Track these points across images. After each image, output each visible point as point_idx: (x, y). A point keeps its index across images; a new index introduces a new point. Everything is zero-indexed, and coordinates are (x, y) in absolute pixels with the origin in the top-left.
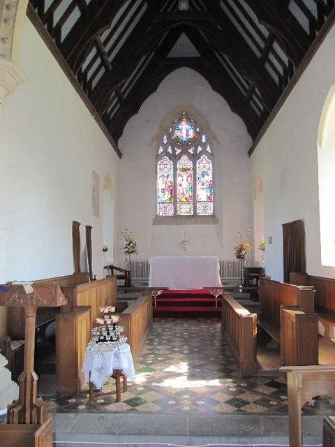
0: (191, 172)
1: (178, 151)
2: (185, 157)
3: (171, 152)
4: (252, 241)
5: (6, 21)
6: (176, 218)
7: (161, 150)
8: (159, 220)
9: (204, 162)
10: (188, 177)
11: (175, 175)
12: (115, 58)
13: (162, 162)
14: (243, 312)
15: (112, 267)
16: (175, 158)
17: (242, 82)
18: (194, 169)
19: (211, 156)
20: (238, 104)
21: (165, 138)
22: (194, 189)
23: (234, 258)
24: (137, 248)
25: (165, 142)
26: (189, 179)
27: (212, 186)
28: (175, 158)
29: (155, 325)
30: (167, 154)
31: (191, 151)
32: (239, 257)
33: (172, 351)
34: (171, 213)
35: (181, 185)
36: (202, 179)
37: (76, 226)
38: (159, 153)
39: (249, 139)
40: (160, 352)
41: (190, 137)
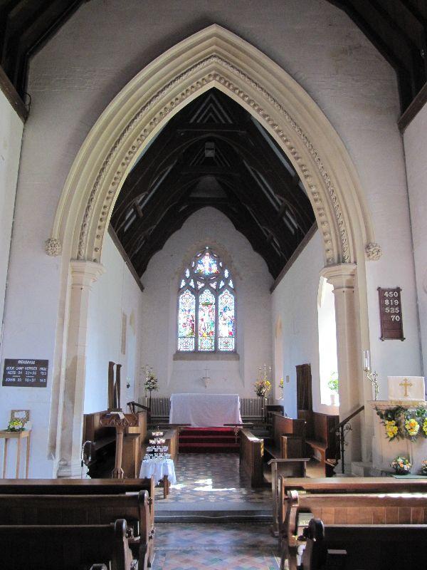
0: (214, 307)
4: (272, 378)
5: (98, 237)
6: (196, 354)
7: (183, 284)
8: (180, 355)
12: (144, 207)
14: (253, 439)
15: (133, 404)
16: (197, 292)
17: (267, 231)
18: (216, 304)
19: (233, 291)
20: (260, 245)
22: (216, 323)
23: (255, 397)
24: (158, 384)
27: (236, 322)
28: (197, 292)
29: (180, 458)
30: (190, 288)
32: (259, 394)
33: (198, 474)
34: (192, 348)
35: (202, 320)
37: (111, 364)
39: (269, 277)
40: (189, 475)
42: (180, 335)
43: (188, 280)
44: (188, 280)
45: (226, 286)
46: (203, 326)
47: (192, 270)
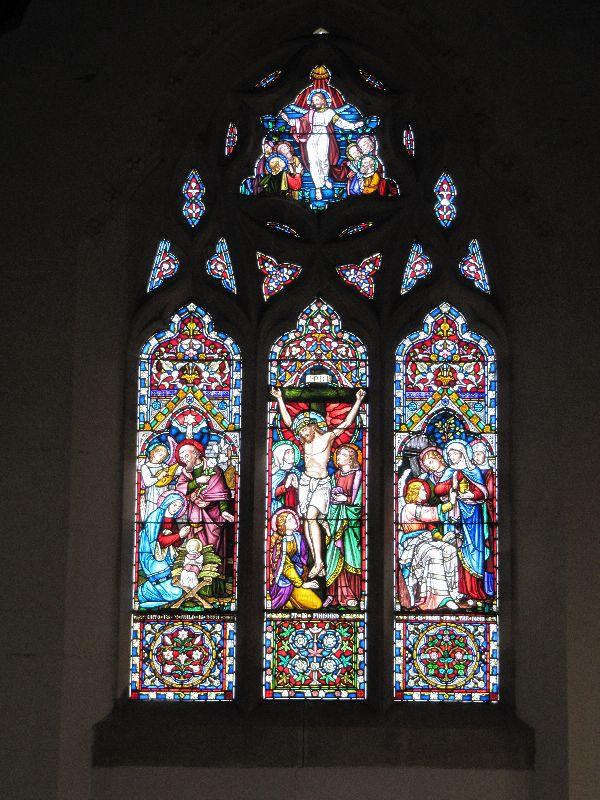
0: (356, 413)
1: (277, 277)
2: (318, 315)
3: (230, 283)
6: (250, 724)
7: (164, 265)
8: (142, 732)
9: (445, 348)
10: (335, 446)
11: (254, 436)
13: (168, 345)
19: (486, 314)
21: (193, 189)
22: (377, 525)
25: (193, 212)
26: (344, 457)
27: (510, 512)
28: (252, 323)
30: (207, 292)
31: (361, 277)
34: (217, 682)
35: (290, 498)
36: (431, 462)
38: (155, 281)
41: (358, 187)
42: (145, 596)
43: (193, 247)
44: (193, 247)
45: (445, 283)
46: (291, 541)
47: (222, 175)
